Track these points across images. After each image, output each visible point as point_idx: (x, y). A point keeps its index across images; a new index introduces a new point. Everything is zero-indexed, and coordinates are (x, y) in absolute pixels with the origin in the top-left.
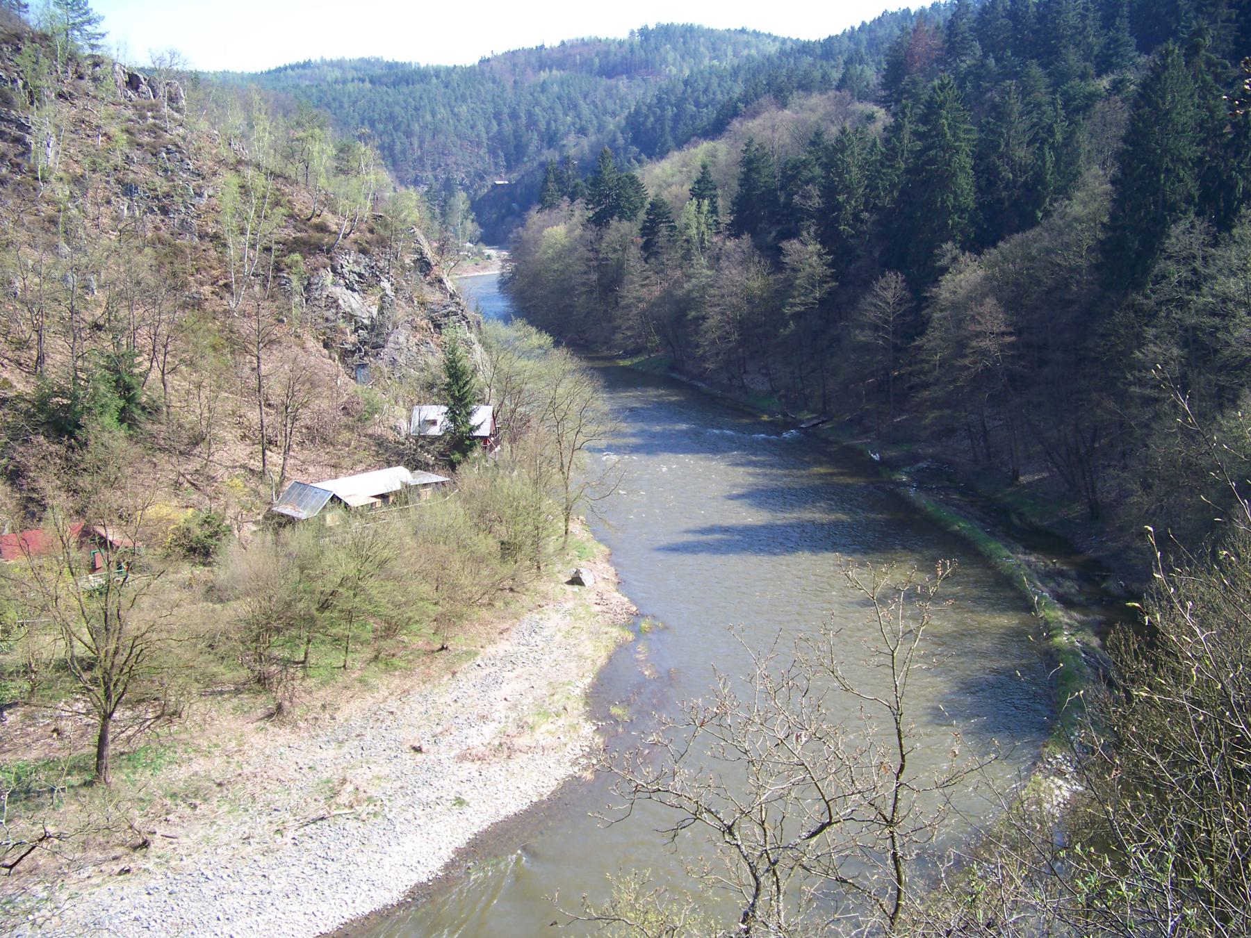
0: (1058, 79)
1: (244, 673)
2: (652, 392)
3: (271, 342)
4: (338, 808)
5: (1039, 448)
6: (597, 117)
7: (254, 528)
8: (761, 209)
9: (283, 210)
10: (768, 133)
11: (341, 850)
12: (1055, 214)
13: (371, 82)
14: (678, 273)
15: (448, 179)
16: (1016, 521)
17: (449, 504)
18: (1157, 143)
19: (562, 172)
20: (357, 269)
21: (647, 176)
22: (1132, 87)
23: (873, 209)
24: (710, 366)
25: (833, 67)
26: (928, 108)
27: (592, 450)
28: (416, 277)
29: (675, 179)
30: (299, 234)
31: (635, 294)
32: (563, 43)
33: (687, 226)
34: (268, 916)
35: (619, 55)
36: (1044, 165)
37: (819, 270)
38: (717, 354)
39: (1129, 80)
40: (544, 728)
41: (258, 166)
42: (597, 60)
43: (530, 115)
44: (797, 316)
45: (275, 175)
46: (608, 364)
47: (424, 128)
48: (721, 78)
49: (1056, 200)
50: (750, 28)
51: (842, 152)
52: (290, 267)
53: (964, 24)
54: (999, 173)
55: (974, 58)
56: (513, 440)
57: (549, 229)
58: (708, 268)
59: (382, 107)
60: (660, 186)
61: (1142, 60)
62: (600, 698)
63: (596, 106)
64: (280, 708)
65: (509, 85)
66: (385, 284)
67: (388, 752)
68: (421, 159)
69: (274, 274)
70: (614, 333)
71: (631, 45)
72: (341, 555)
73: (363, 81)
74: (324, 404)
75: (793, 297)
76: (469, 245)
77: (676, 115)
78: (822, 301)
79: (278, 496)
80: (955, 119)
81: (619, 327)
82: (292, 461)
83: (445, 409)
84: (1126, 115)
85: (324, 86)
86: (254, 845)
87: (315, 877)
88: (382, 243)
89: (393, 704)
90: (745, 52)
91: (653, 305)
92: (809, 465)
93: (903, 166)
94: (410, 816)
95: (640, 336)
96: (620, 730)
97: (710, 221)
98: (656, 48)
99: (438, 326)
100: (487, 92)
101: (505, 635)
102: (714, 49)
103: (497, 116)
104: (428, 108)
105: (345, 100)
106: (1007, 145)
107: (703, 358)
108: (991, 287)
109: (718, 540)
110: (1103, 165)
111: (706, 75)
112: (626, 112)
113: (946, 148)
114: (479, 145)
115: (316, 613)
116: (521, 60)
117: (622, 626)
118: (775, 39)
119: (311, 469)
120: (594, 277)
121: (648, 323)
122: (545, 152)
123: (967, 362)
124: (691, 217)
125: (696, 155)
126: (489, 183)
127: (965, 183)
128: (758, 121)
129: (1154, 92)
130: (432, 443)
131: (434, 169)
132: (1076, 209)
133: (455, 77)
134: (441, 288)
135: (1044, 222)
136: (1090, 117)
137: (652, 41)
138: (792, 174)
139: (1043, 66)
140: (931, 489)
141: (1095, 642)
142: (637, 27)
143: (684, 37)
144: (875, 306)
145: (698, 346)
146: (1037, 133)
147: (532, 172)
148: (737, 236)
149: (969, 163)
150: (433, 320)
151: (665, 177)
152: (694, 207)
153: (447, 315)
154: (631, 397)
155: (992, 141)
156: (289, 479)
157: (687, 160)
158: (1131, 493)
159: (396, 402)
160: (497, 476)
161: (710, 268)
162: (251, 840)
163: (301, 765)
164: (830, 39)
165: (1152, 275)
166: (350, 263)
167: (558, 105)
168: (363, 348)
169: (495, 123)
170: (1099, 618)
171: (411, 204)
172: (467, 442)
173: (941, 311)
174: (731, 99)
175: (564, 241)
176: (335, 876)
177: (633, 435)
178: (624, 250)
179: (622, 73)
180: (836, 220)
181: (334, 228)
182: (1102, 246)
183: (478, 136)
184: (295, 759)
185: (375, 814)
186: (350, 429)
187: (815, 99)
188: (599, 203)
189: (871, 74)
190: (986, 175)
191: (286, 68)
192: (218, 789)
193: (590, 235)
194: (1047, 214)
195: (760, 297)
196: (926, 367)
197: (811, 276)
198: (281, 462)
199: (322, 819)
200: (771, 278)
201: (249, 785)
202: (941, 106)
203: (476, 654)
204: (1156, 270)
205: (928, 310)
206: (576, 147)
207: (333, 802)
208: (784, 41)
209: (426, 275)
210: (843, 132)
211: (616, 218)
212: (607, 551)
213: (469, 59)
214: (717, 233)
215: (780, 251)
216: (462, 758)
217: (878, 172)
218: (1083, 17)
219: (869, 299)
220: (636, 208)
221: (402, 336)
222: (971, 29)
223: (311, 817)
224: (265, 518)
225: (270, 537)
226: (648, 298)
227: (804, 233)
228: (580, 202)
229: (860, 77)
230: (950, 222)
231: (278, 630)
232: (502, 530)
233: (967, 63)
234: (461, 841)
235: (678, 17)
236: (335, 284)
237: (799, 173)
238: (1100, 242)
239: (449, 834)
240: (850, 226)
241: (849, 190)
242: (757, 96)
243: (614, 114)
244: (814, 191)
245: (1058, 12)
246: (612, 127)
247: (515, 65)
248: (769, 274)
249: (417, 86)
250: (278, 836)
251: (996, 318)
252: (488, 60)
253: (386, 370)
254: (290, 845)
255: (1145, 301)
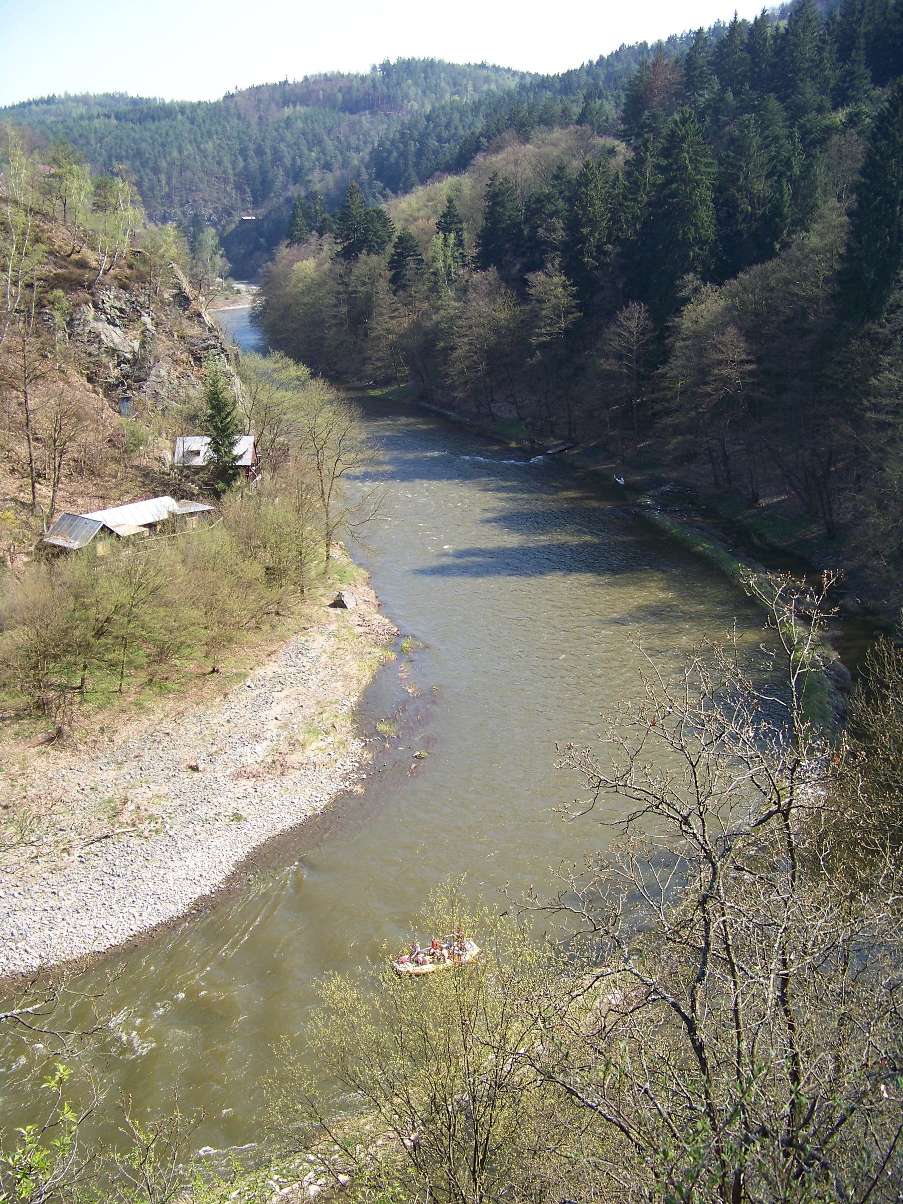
0: (796, 113)
1: (25, 699)
2: (403, 420)
3: (37, 378)
4: (120, 827)
5: (779, 471)
6: (341, 153)
7: (26, 559)
8: (506, 241)
9: (43, 247)
10: (512, 167)
11: (126, 866)
12: (793, 246)
13: (117, 118)
14: (426, 305)
15: (196, 215)
16: (756, 541)
17: (215, 532)
18: (893, 175)
19: (309, 207)
20: (117, 304)
21: (392, 210)
22: (868, 120)
23: (616, 241)
24: (459, 395)
25: (573, 101)
26: (669, 142)
27: (348, 477)
28: (176, 311)
29: (421, 213)
30: (59, 271)
31: (385, 326)
32: (306, 78)
33: (434, 259)
34: (60, 931)
35: (362, 91)
36: (782, 197)
37: (564, 301)
38: (466, 383)
39: (864, 113)
40: (314, 745)
41: (16, 202)
42: (340, 96)
43: (275, 151)
44: (542, 346)
45: (30, 211)
46: (359, 395)
47: (172, 164)
48: (463, 113)
49: (794, 232)
50: (490, 63)
51: (586, 186)
52: (53, 303)
53: (702, 58)
54: (738, 206)
55: (711, 92)
56: (275, 468)
57: (299, 264)
58: (455, 300)
59: (126, 140)
60: (406, 220)
61: (878, 92)
62: (367, 714)
63: (340, 142)
64: (60, 732)
65: (254, 121)
66: (146, 319)
67: (167, 771)
68: (169, 196)
69: (37, 310)
70: (364, 364)
71: (373, 80)
72: (116, 583)
73: (109, 117)
74: (91, 437)
75: (539, 328)
76: (219, 280)
77: (420, 150)
78: (567, 331)
79: (48, 528)
80: (696, 153)
81: (369, 358)
82: (61, 493)
83: (209, 440)
84: (861, 148)
85: (70, 123)
86: (42, 864)
87: (102, 893)
88: (141, 278)
89: (168, 726)
90: (486, 87)
91: (401, 336)
92: (558, 489)
93: (645, 199)
94: (190, 832)
95: (389, 368)
96: (387, 745)
97: (457, 254)
98: (398, 84)
99: (198, 359)
100: (232, 128)
101: (273, 657)
102: (455, 84)
103: (243, 152)
104: (175, 144)
105: (92, 136)
106: (746, 178)
107: (453, 388)
108: (729, 317)
109: (473, 562)
110: (840, 199)
111: (448, 109)
112: (370, 148)
113: (687, 181)
114: (226, 181)
115: (92, 640)
116: (266, 95)
117: (385, 647)
118: (515, 74)
119: (80, 501)
120: (344, 309)
121: (397, 354)
122: (291, 187)
123: (709, 389)
124: (438, 250)
125: (441, 190)
126: (237, 219)
127: (706, 215)
128: (500, 157)
129: (892, 125)
130: (197, 473)
131: (182, 205)
132: (813, 240)
133: (200, 113)
134: (200, 322)
135: (783, 254)
136: (826, 151)
137: (394, 76)
138: (536, 208)
139: (781, 100)
140: (675, 511)
141: (835, 656)
142: (379, 62)
143: (425, 72)
144: (619, 335)
145: (447, 375)
146: (775, 166)
147: (279, 207)
148: (484, 268)
149: (709, 195)
150: (193, 354)
151: (410, 210)
152: (440, 241)
153: (206, 349)
154: (385, 426)
155: (731, 174)
156: (58, 511)
157: (432, 194)
158: (865, 515)
159: (160, 434)
160: (261, 502)
161: (458, 299)
162: (39, 859)
163: (83, 786)
164: (569, 73)
165: (887, 304)
166: (110, 298)
167: (303, 141)
168: (127, 380)
169: (241, 159)
170: (838, 633)
171: (169, 241)
172: (231, 472)
173: (683, 340)
174: (473, 133)
175: (313, 275)
176: (122, 891)
177: (388, 463)
178: (372, 284)
179: (365, 109)
180: (581, 252)
181: (94, 264)
182: (839, 277)
183: (225, 172)
184: (76, 781)
185: (157, 832)
186: (117, 461)
187: (557, 133)
188: (347, 238)
189: (610, 109)
190: (726, 209)
191: (30, 103)
192: (5, 811)
193: (339, 269)
194: (785, 246)
195: (507, 328)
196: (669, 394)
197: (556, 307)
198: (51, 494)
199: (106, 837)
200: (517, 309)
201: (34, 807)
202: (683, 139)
203: (246, 676)
204: (891, 300)
205: (671, 339)
206: (322, 182)
207: (116, 821)
208: (523, 76)
209: (185, 309)
210: (587, 166)
211: (364, 251)
212: (367, 575)
213: (213, 94)
214: (463, 266)
215: (525, 283)
216: (238, 776)
217: (621, 205)
218: (820, 50)
219: (613, 328)
220: (384, 242)
221: (163, 370)
222: (709, 63)
223: (96, 835)
224: (37, 549)
225: (44, 567)
226: (397, 329)
227: (549, 265)
228: (328, 237)
229: (600, 111)
230: (691, 253)
231: (55, 657)
232: (266, 557)
233: (705, 96)
234: (240, 853)
235: (419, 52)
236: (97, 319)
237: (543, 206)
238: (839, 273)
239: (228, 848)
240: (592, 257)
241: (593, 223)
242: (499, 131)
243: (357, 150)
244: (559, 224)
245: (796, 45)
246: (356, 162)
247: (259, 101)
248: (514, 305)
249: (163, 123)
250: (65, 855)
251: (736, 347)
252: (233, 96)
253: (149, 402)
254: (76, 863)
255: (880, 330)
